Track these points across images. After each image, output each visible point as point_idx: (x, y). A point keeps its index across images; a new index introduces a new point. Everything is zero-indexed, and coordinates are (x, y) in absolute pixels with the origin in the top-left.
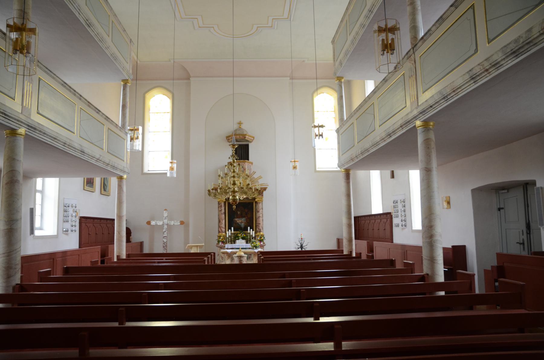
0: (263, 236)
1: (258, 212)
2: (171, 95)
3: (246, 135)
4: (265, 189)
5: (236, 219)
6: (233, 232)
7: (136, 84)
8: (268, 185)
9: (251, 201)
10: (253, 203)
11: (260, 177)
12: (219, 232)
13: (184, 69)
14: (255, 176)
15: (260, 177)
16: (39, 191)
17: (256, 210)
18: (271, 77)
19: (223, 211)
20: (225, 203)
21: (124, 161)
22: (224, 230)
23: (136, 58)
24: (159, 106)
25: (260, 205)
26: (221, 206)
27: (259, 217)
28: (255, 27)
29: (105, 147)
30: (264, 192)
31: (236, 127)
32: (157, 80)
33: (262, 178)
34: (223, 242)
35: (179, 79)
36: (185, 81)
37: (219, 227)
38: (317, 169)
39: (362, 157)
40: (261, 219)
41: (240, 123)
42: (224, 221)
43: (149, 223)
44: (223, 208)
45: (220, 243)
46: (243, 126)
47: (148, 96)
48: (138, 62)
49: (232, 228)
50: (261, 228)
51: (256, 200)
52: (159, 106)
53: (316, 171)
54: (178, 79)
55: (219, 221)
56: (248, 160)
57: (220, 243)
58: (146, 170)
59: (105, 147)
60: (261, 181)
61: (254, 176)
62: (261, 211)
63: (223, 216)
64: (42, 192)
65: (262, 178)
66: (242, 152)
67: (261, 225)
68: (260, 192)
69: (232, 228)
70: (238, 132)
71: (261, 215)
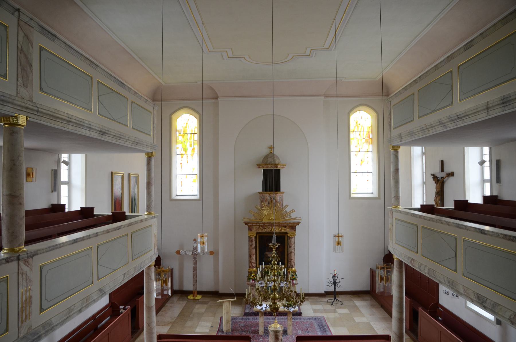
0: (295, 272)
1: (290, 247)
2: (198, 116)
3: (278, 164)
4: (298, 224)
5: (267, 253)
6: (264, 266)
7: (165, 100)
8: (301, 220)
9: (284, 235)
10: (284, 236)
11: (293, 211)
12: (250, 267)
13: (212, 89)
14: (288, 210)
15: (293, 211)
16: (65, 183)
17: (288, 243)
18: (304, 96)
19: (254, 245)
20: (256, 237)
21: (150, 135)
22: (254, 265)
23: (161, 81)
24: (186, 124)
25: (293, 240)
26: (252, 241)
27: (291, 252)
28: (290, 56)
29: (129, 123)
30: (297, 227)
31: (265, 151)
32: (184, 100)
33: (294, 211)
34: (254, 280)
35: (206, 100)
36: (213, 101)
37: (250, 262)
38: (353, 196)
39: (451, 126)
40: (293, 254)
41: (271, 148)
42: (255, 256)
43: (178, 252)
44: (254, 243)
45: (251, 281)
46: (276, 152)
47: (174, 117)
48: (163, 84)
49: (263, 263)
50: (293, 264)
51: (289, 235)
52: (186, 124)
53: (351, 198)
54: (206, 99)
55: (250, 256)
56: (280, 191)
57: (251, 281)
58: (174, 196)
59: (129, 123)
60: (293, 215)
61: (286, 210)
62: (293, 246)
63: (254, 250)
64: (68, 183)
65: (294, 211)
66: (272, 180)
67: (293, 261)
68: (293, 227)
69: (263, 263)
70: (270, 160)
71: (293, 251)
